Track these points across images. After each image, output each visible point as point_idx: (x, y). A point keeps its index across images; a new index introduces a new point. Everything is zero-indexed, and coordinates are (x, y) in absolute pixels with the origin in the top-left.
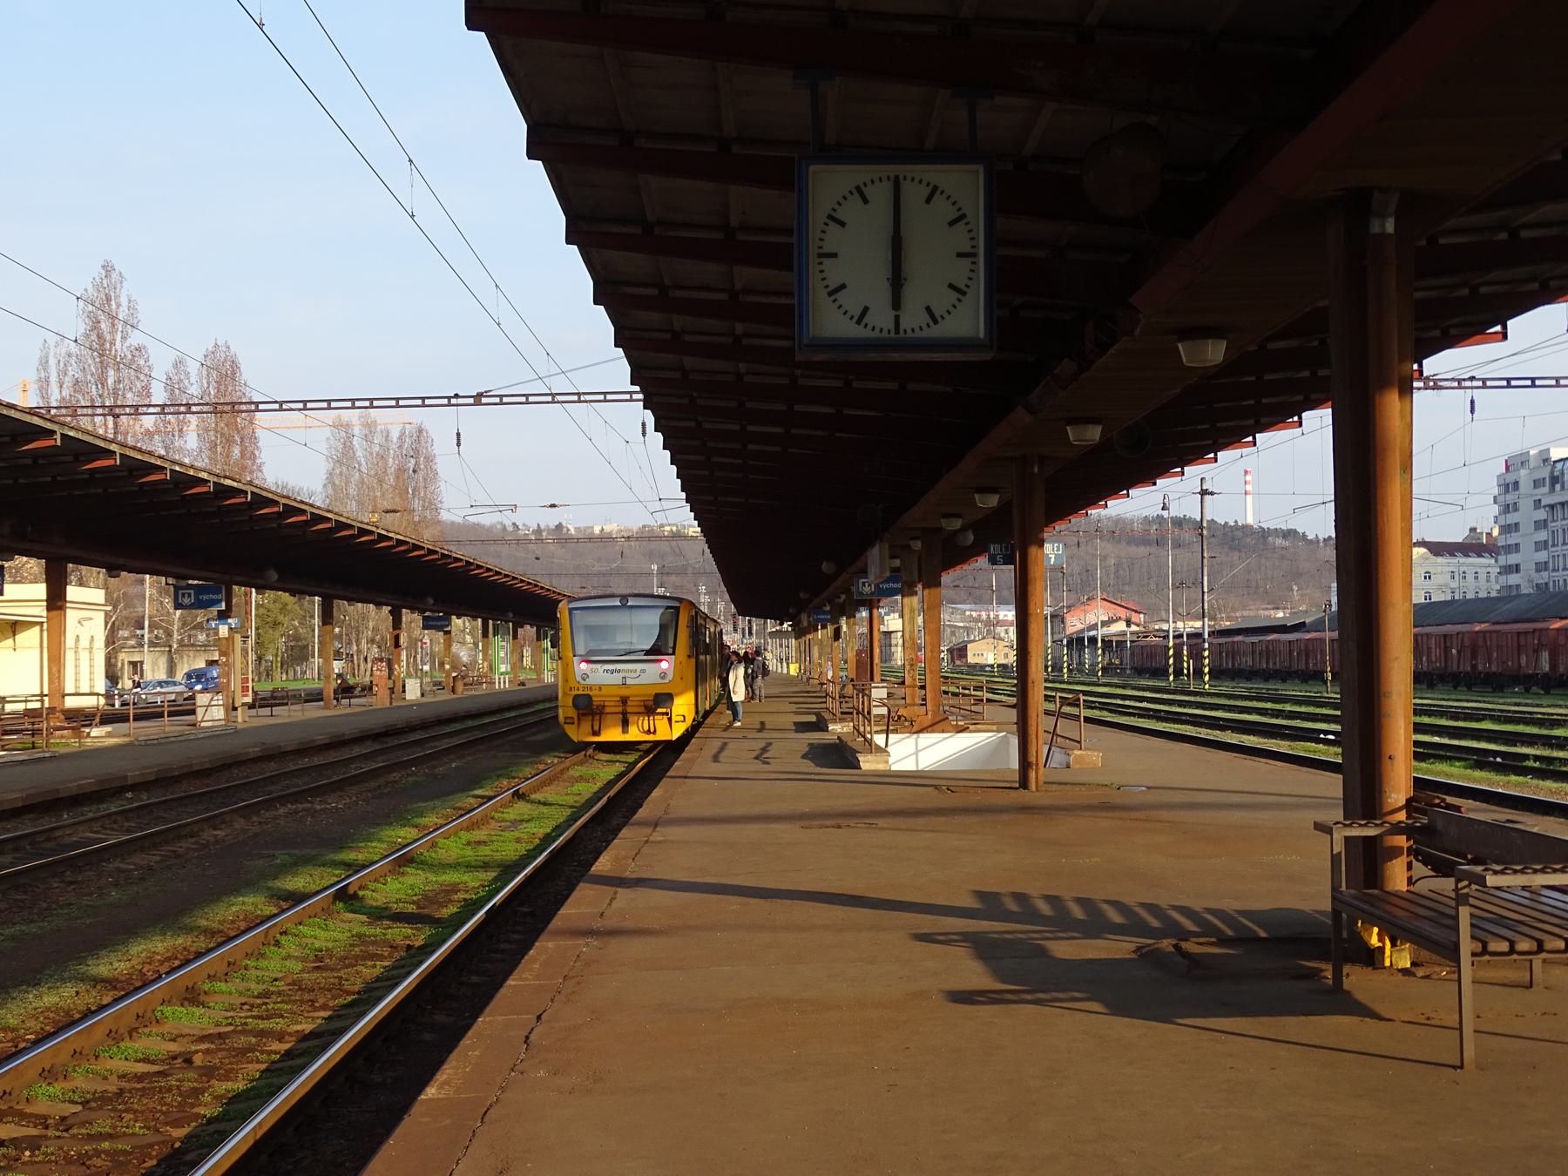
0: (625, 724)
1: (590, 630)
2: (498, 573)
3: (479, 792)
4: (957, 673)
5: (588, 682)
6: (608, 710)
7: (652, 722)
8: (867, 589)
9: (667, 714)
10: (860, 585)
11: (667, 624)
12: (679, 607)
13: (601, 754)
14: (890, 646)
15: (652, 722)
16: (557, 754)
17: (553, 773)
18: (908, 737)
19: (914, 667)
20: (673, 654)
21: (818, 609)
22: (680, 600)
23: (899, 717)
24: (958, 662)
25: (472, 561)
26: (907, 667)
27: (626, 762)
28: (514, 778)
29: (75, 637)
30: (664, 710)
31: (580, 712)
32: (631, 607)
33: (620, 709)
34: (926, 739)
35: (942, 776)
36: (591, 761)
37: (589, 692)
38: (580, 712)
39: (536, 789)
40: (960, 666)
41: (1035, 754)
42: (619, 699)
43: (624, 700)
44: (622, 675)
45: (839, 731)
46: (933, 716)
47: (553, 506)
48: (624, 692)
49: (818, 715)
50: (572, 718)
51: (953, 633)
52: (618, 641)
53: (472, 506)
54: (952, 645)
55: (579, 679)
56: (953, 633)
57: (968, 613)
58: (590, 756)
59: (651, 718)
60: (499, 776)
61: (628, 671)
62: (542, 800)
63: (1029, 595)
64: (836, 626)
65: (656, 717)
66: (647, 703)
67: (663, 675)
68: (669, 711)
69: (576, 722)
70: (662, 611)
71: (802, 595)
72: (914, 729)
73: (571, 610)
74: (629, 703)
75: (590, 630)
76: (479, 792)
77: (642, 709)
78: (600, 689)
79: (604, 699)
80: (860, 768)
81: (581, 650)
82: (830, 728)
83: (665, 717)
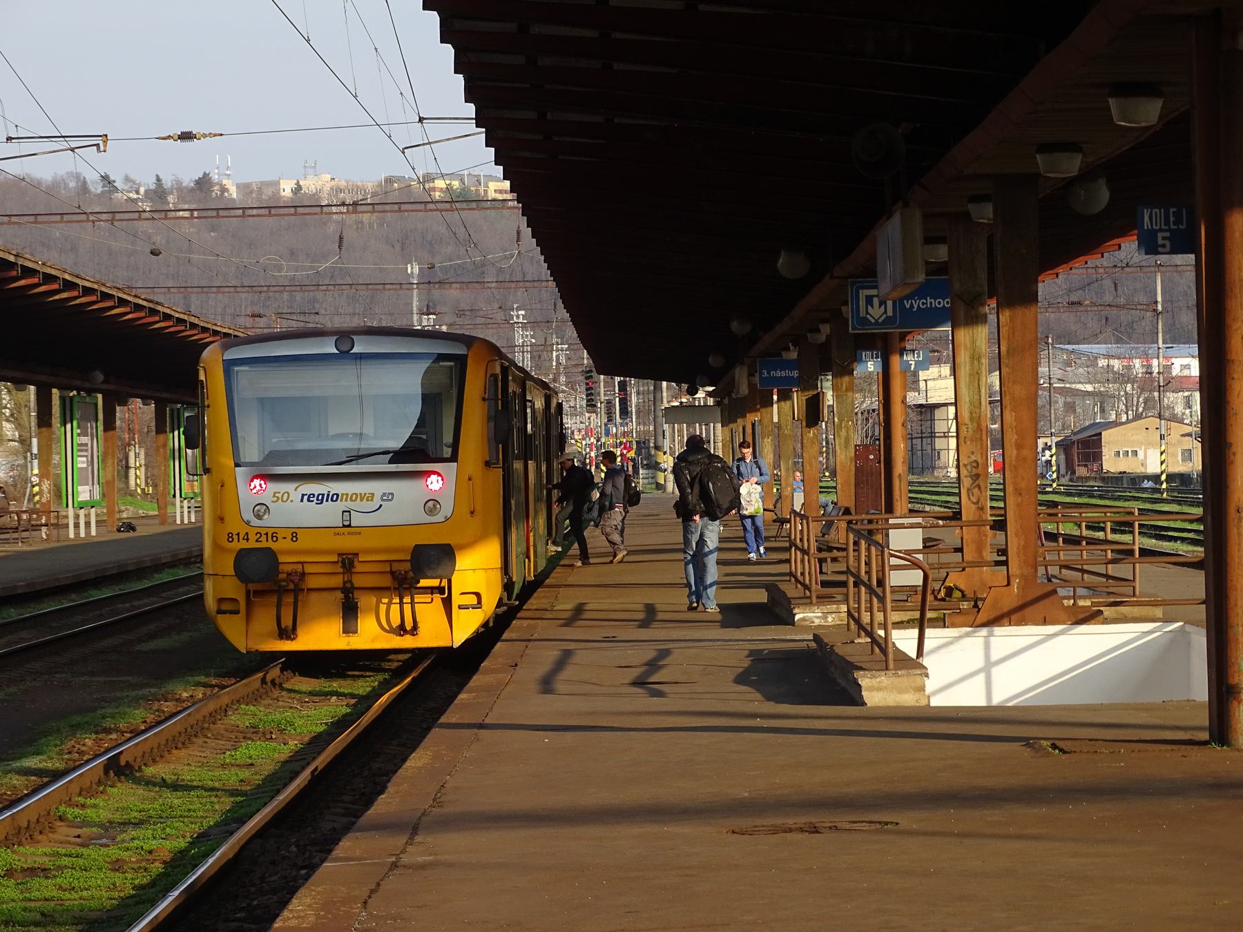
0: (350, 612)
1: (270, 406)
2: (69, 285)
3: (31, 762)
4: (1080, 495)
5: (269, 521)
6: (312, 582)
7: (407, 608)
8: (876, 312)
9: (440, 590)
10: (862, 303)
11: (439, 395)
12: (466, 356)
13: (298, 678)
14: (932, 435)
15: (407, 608)
16: (202, 679)
17: (192, 721)
18: (967, 635)
19: (981, 482)
20: (454, 458)
21: (773, 356)
22: (468, 341)
23: (949, 591)
24: (1081, 471)
25: (12, 259)
26: (967, 482)
27: (352, 696)
28: (108, 731)
30: (434, 583)
31: (252, 587)
32: (361, 357)
33: (337, 581)
34: (1007, 638)
35: (1051, 717)
36: (276, 693)
37: (271, 544)
38: (252, 587)
39: (154, 756)
40: (1087, 479)
42: (335, 558)
43: (347, 561)
44: (341, 505)
45: (817, 622)
46: (1022, 588)
47: (186, 136)
48: (348, 543)
49: (771, 588)
50: (234, 600)
51: (1070, 408)
52: (332, 431)
53: (9, 139)
54: (1068, 432)
55: (248, 515)
56: (1070, 408)
57: (1102, 363)
58: (273, 682)
59: (407, 599)
60: (75, 728)
61: (354, 497)
62: (169, 778)
63: (1229, 321)
64: (811, 393)
65: (418, 598)
66: (396, 567)
67: (432, 505)
68: (445, 583)
69: (243, 606)
70: (424, 365)
71: (735, 326)
72: (982, 617)
73: (229, 365)
74: (359, 567)
75: (270, 406)
76: (31, 762)
77: (386, 581)
78: (294, 537)
79: (302, 560)
80: (864, 704)
81: (251, 452)
82: (797, 617)
83: (438, 598)
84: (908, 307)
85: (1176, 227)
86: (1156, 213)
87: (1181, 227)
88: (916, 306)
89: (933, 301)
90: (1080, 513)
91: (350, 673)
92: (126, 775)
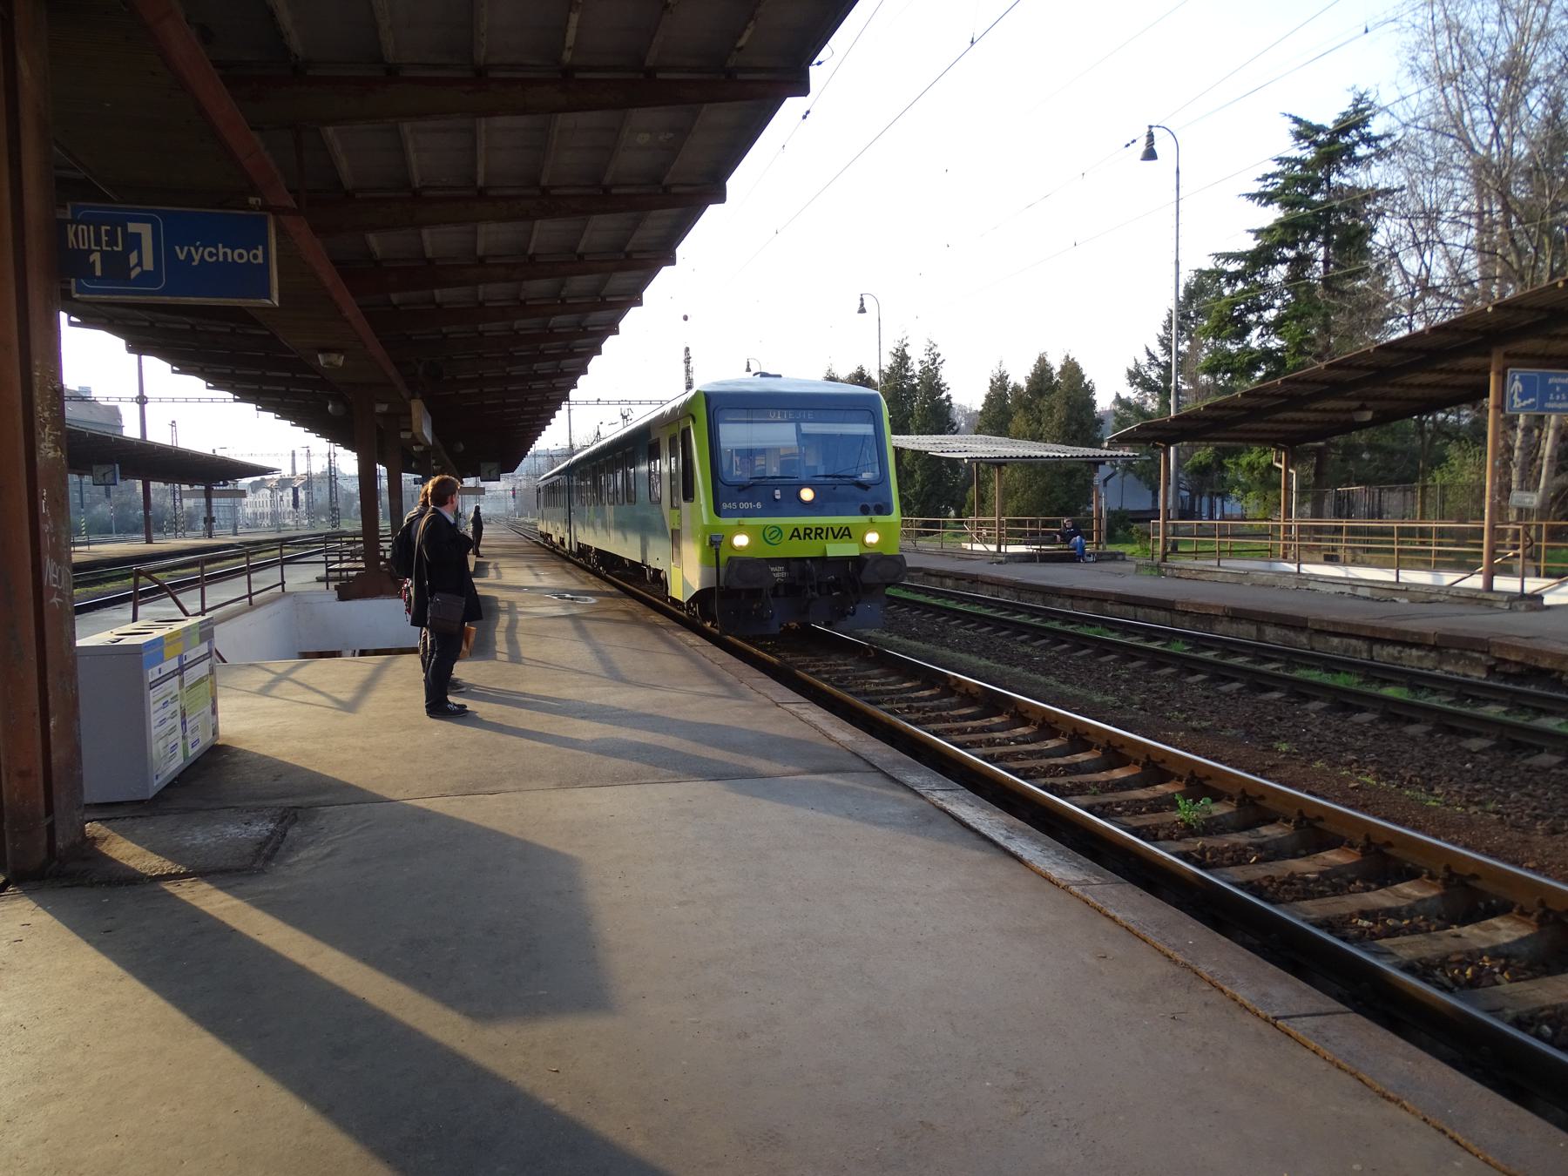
29: (291, 453)
41: (1015, 846)
84: (182, 257)
85: (109, 249)
86: (83, 230)
87: (115, 248)
88: (197, 258)
89: (229, 251)
90: (326, 556)
91: (1243, 413)
92: (1293, 181)
